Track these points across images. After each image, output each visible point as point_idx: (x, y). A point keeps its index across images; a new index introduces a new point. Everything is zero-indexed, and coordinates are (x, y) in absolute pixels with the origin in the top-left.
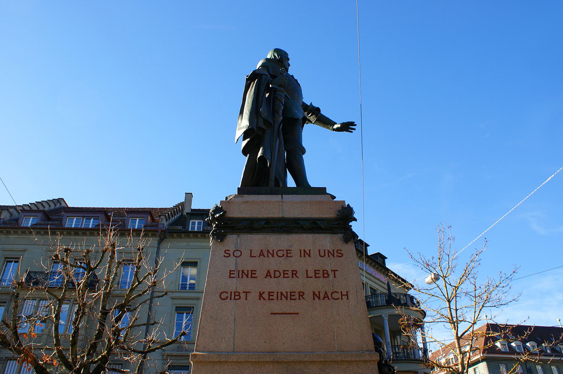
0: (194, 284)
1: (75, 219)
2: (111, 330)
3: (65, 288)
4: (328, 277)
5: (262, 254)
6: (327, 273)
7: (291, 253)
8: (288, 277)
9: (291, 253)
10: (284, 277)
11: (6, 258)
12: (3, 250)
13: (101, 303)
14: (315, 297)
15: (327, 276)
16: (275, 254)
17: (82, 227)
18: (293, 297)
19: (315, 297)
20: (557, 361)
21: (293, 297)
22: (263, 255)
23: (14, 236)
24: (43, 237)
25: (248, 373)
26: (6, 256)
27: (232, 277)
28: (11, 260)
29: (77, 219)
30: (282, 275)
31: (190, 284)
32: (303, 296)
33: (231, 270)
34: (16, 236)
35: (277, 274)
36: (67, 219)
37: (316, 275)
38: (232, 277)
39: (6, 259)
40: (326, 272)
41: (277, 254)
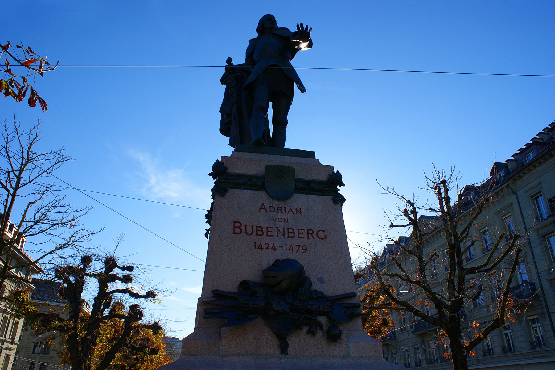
0: (418, 350)
1: (531, 154)
5: (263, 207)
11: (532, 197)
12: (526, 192)
13: (553, 260)
14: (297, 212)
17: (469, 251)
18: (269, 234)
19: (297, 212)
21: (269, 234)
22: (265, 208)
23: (526, 177)
24: (546, 163)
25: (418, 364)
26: (532, 195)
28: (537, 196)
29: (532, 153)
31: (419, 350)
34: (527, 176)
36: (525, 159)
39: (533, 197)
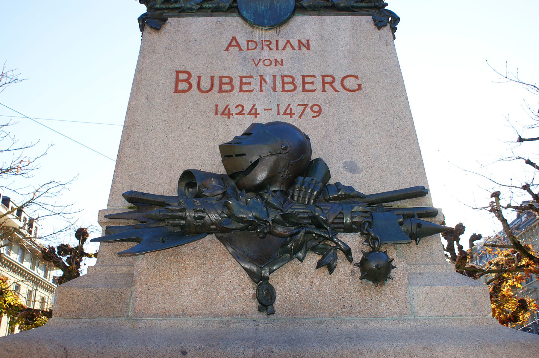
2: (175, 300)
3: (57, 256)
4: (231, 91)
6: (230, 83)
7: (312, 83)
8: (251, 91)
9: (312, 83)
10: (241, 90)
15: (292, 87)
16: (273, 61)
20: (131, 227)
22: (238, 45)
27: (247, 91)
30: (300, 88)
32: (333, 84)
33: (180, 69)
35: (205, 84)
37: (223, 86)
38: (247, 91)
40: (183, 76)
41: (271, 62)
